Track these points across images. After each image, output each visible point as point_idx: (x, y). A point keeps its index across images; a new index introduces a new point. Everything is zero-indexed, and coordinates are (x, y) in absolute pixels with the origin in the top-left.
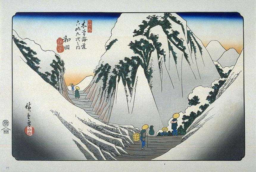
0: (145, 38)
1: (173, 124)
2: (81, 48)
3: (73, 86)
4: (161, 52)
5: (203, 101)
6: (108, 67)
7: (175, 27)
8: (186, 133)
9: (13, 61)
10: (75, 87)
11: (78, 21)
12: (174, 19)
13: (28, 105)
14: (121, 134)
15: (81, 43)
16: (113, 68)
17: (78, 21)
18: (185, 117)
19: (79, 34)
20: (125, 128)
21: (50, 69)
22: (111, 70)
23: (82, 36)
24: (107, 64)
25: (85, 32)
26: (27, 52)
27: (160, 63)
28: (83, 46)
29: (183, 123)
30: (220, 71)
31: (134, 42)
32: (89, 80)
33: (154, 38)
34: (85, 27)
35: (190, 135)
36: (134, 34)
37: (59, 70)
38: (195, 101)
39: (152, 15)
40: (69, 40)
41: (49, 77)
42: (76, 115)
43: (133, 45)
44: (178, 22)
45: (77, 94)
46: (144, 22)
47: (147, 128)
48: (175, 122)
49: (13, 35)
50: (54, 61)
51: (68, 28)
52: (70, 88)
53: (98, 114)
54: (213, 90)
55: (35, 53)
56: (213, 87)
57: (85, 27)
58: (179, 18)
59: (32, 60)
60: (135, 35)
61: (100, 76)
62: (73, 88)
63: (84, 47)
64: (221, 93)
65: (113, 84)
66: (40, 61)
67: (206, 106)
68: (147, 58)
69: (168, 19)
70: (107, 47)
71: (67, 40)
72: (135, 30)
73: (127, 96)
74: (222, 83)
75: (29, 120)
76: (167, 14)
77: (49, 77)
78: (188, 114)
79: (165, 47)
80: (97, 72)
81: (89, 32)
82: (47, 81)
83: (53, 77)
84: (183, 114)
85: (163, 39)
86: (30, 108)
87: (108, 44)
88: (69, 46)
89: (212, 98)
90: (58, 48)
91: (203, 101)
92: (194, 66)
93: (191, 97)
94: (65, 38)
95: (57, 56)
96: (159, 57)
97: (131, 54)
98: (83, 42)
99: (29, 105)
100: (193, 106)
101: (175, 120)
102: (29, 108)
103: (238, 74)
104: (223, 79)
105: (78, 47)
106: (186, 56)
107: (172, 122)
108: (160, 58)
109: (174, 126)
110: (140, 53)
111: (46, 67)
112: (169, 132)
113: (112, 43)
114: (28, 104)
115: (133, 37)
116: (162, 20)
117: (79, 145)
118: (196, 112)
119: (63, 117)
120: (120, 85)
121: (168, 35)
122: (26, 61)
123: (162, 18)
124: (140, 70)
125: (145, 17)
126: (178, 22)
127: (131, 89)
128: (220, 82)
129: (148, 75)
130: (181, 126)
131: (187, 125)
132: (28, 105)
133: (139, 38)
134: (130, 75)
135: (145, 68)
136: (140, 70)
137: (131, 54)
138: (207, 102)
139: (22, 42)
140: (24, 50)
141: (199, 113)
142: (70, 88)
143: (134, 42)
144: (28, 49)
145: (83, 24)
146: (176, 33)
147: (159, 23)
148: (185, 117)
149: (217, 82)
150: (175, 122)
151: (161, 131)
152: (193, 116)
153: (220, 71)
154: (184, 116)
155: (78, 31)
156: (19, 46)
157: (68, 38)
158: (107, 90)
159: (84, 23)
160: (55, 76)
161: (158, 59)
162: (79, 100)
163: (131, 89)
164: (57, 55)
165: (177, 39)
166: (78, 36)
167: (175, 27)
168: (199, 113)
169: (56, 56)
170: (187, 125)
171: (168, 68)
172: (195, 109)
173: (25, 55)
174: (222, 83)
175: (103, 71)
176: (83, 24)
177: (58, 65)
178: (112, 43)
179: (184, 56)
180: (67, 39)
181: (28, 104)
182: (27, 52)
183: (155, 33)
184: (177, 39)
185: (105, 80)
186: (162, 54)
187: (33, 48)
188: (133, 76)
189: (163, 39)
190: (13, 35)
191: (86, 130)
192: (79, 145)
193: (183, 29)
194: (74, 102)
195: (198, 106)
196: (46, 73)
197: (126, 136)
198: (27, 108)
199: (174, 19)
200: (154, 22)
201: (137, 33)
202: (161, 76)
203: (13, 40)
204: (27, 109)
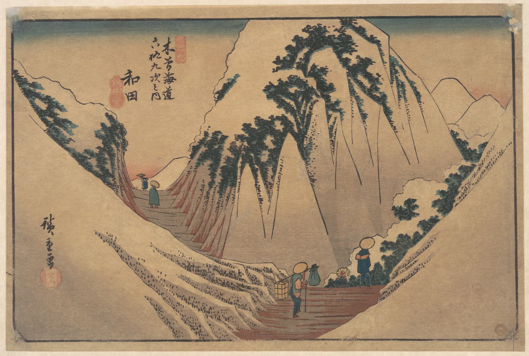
0: (300, 74)
1: (360, 262)
2: (163, 97)
3: (142, 176)
4: (332, 107)
5: (426, 211)
6: (218, 139)
7: (363, 49)
8: (388, 281)
9: (15, 123)
10: (149, 181)
11: (155, 38)
12: (361, 31)
13: (48, 220)
14: (249, 283)
15: (162, 88)
16: (231, 139)
17: (155, 38)
18: (386, 245)
19: (158, 67)
20: (257, 270)
21: (95, 144)
22: (227, 145)
23: (163, 71)
24: (216, 133)
25: (172, 62)
26: (43, 106)
27: (331, 129)
28: (166, 94)
29: (384, 257)
30: (461, 144)
31: (276, 83)
32: (179, 167)
33: (318, 73)
34: (170, 52)
35: (397, 286)
36: (275, 66)
37: (113, 146)
38: (407, 211)
39: (313, 23)
40: (136, 80)
41: (93, 162)
42: (150, 240)
43: (272, 90)
44: (372, 39)
45: (155, 197)
46: (297, 39)
47: (305, 271)
48: (364, 257)
49: (14, 69)
50: (103, 125)
51: (135, 54)
52: (137, 184)
53: (198, 239)
54: (445, 187)
55: (61, 109)
56: (447, 181)
57: (170, 52)
58: (371, 30)
59: (56, 125)
60: (278, 69)
61: (204, 157)
62: (145, 185)
63: (168, 95)
64: (464, 195)
65: (230, 178)
66: (75, 126)
67: (434, 221)
68: (306, 120)
69: (349, 32)
70: (218, 95)
71: (133, 79)
72: (278, 58)
73: (261, 200)
74: (466, 171)
75: (50, 254)
76: (347, 22)
77: (93, 162)
78: (392, 237)
79: (341, 94)
80: (195, 149)
81: (178, 62)
82: (88, 168)
83: (101, 161)
84: (382, 240)
85: (337, 75)
86: (53, 227)
87: (220, 88)
88: (136, 92)
89: (446, 203)
90: (112, 98)
91: (426, 211)
92: (403, 134)
93: (399, 202)
94: (128, 75)
95: (112, 116)
96: (329, 117)
97: (270, 109)
98: (167, 85)
99: (51, 220)
100: (403, 221)
101: (365, 252)
102: (51, 228)
103: (501, 153)
104: (469, 164)
105: (155, 95)
106: (388, 112)
107: (358, 257)
108: (332, 120)
109: (363, 264)
110: (288, 108)
111: (86, 138)
112: (353, 277)
113: (227, 87)
114: (47, 218)
115: (273, 72)
116: (337, 34)
117: (158, 309)
118: (411, 235)
119: (124, 247)
120: (246, 178)
121: (348, 68)
122: (45, 127)
123: (336, 30)
124: (290, 141)
125: (297, 29)
126: (372, 39)
127: (269, 186)
128: (461, 168)
129: (304, 152)
130: (377, 265)
131: (391, 262)
132: (48, 220)
133: (284, 75)
134: (265, 157)
135: (300, 137)
136: (290, 141)
137: (270, 109)
138: (434, 212)
139: (34, 85)
140: (38, 102)
141: (417, 238)
142: (137, 184)
143: (276, 83)
144: (47, 99)
145: (167, 46)
146: (366, 62)
147: (329, 41)
148: (386, 245)
149: (455, 170)
150: (364, 257)
151: (334, 277)
152: (405, 242)
153: (461, 144)
154: (385, 243)
155: (155, 60)
156: (28, 94)
157: (134, 75)
158: (218, 189)
159: (169, 42)
160: (106, 155)
161: (328, 122)
162: (159, 210)
163: (269, 186)
164: (110, 113)
165: (368, 76)
166: (155, 71)
167: (363, 49)
168: (417, 238)
169: (107, 115)
170: (391, 262)
171: (349, 140)
172: (409, 227)
173: (40, 113)
174: (466, 171)
175: (209, 148)
176: (167, 46)
177: (113, 134)
178: (227, 87)
179: (383, 114)
180: (133, 77)
181: (47, 218)
182: (43, 106)
183: (320, 65)
184: (368, 76)
185: (213, 169)
186: (335, 110)
187: (60, 97)
188: (275, 154)
189: (337, 75)
190: (14, 69)
191: (171, 272)
192: (158, 309)
193: (382, 54)
194: (147, 215)
195: (415, 220)
196: (86, 151)
197: (259, 287)
198: (47, 226)
199: (361, 31)
200: (317, 39)
201: (282, 64)
202: (334, 157)
203: (15, 81)
204: (46, 230)
